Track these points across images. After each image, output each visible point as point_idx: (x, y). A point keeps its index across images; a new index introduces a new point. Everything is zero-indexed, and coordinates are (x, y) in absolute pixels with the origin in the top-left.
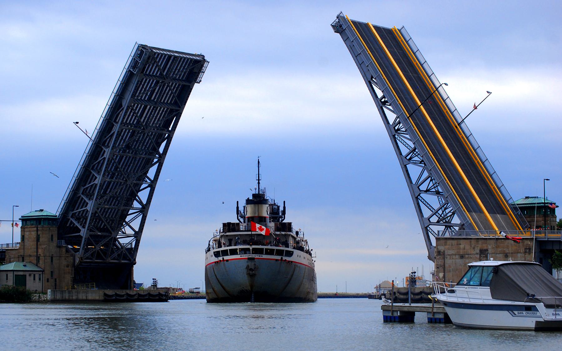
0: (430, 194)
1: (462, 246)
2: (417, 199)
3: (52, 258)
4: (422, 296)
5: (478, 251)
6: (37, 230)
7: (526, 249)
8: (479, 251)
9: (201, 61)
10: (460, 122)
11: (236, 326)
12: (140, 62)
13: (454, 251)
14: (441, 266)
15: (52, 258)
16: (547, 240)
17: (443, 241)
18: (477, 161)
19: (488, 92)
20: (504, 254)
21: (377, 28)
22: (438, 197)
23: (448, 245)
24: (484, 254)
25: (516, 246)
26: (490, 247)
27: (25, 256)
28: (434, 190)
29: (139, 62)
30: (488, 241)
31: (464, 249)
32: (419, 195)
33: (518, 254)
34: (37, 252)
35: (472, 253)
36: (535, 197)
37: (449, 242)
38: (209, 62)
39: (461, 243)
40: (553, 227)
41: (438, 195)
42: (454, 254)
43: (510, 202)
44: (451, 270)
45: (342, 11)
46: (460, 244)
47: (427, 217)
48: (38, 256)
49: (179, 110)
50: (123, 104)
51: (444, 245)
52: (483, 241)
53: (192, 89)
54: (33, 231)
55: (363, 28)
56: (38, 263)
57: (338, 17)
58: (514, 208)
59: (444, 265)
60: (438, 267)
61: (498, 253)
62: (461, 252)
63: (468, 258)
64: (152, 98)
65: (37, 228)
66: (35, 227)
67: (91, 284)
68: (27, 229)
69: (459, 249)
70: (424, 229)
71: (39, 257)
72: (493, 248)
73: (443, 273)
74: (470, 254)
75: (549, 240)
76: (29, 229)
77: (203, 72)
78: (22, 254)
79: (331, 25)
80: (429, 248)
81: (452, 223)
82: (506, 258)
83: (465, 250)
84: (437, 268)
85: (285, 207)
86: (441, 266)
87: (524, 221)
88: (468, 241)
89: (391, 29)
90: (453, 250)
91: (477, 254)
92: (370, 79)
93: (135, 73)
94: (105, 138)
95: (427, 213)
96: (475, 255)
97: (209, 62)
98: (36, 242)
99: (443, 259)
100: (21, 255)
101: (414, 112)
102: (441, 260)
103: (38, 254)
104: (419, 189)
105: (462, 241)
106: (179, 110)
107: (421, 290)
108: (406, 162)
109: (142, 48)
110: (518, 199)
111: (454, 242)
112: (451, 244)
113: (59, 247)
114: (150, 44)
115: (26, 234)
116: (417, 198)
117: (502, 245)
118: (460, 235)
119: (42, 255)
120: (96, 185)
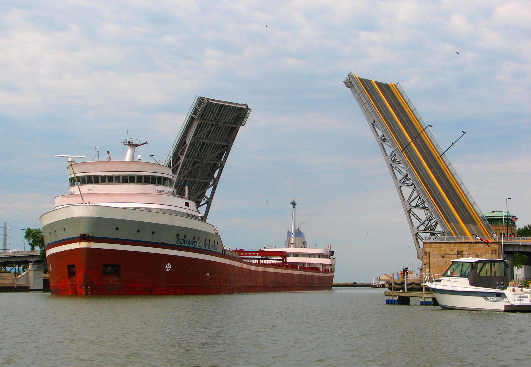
1: (443, 249)
5: (456, 252)
7: (492, 251)
9: (245, 109)
12: (200, 110)
13: (437, 252)
21: (378, 84)
22: (425, 211)
24: (460, 255)
26: (464, 249)
28: (421, 206)
31: (445, 251)
37: (434, 245)
38: (251, 110)
41: (425, 210)
43: (480, 215)
46: (442, 247)
49: (229, 146)
55: (366, 83)
57: (348, 76)
63: (448, 257)
77: (246, 117)
83: (446, 252)
88: (448, 244)
90: (437, 251)
92: (372, 122)
93: (196, 118)
95: (416, 223)
97: (251, 110)
108: (400, 185)
109: (201, 99)
110: (487, 213)
114: (207, 96)
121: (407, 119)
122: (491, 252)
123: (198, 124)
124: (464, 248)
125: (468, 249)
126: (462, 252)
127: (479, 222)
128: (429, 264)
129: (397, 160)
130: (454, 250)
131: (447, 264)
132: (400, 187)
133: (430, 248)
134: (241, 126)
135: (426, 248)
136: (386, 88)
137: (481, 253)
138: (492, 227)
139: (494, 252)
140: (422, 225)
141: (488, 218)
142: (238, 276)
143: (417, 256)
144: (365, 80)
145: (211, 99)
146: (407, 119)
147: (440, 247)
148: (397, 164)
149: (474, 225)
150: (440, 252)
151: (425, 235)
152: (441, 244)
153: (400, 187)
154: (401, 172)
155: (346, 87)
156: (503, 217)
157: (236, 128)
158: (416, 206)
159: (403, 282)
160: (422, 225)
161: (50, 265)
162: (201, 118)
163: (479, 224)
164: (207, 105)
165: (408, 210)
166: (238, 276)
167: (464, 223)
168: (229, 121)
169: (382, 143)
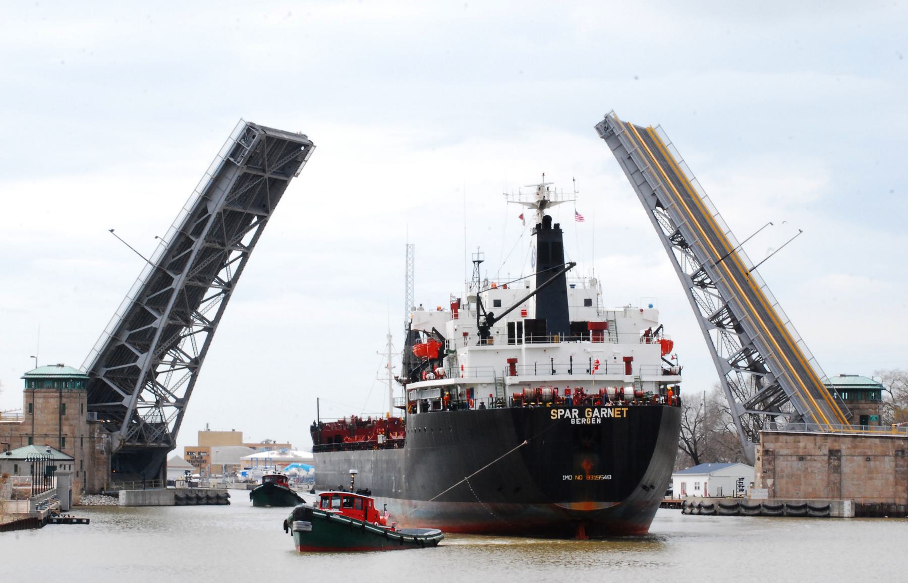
1: (802, 445)
3: (82, 438)
4: (761, 510)
5: (826, 452)
6: (61, 397)
7: (897, 451)
12: (249, 148)
13: (789, 450)
15: (82, 438)
17: (772, 437)
18: (779, 323)
19: (800, 230)
20: (866, 457)
23: (781, 442)
24: (835, 456)
26: (843, 447)
27: (34, 436)
29: (247, 149)
30: (842, 439)
31: (805, 448)
33: (886, 457)
34: (60, 430)
35: (817, 454)
36: (856, 376)
37: (782, 438)
39: (801, 441)
40: (592, 374)
42: (790, 454)
44: (785, 476)
45: (660, 124)
46: (799, 442)
48: (62, 436)
50: (210, 210)
51: (774, 441)
52: (834, 438)
54: (52, 398)
56: (62, 448)
60: (765, 471)
61: (856, 455)
62: (801, 452)
63: (810, 460)
65: (61, 393)
66: (56, 392)
67: (135, 483)
68: (39, 394)
69: (798, 448)
71: (64, 439)
72: (848, 448)
73: (773, 480)
74: (815, 456)
76: (43, 394)
77: (305, 161)
78: (29, 431)
82: (869, 462)
83: (806, 450)
84: (764, 472)
85: (520, 382)
88: (812, 438)
90: (789, 448)
91: (825, 455)
94: (173, 258)
96: (822, 457)
98: (58, 415)
100: (27, 434)
103: (62, 433)
105: (801, 438)
106: (266, 217)
107: (760, 503)
111: (790, 439)
112: (785, 441)
113: (90, 422)
114: (259, 122)
115: (38, 401)
117: (862, 444)
118: (793, 429)
119: (69, 434)
120: (155, 330)
122: (894, 453)
124: (842, 445)
126: (839, 451)
128: (774, 471)
130: (823, 447)
137: (874, 454)
138: (846, 404)
141: (837, 387)
142: (871, 498)
147: (795, 442)
149: (822, 401)
150: (796, 450)
152: (796, 437)
156: (454, 313)
161: (609, 477)
166: (871, 498)
167: (814, 398)
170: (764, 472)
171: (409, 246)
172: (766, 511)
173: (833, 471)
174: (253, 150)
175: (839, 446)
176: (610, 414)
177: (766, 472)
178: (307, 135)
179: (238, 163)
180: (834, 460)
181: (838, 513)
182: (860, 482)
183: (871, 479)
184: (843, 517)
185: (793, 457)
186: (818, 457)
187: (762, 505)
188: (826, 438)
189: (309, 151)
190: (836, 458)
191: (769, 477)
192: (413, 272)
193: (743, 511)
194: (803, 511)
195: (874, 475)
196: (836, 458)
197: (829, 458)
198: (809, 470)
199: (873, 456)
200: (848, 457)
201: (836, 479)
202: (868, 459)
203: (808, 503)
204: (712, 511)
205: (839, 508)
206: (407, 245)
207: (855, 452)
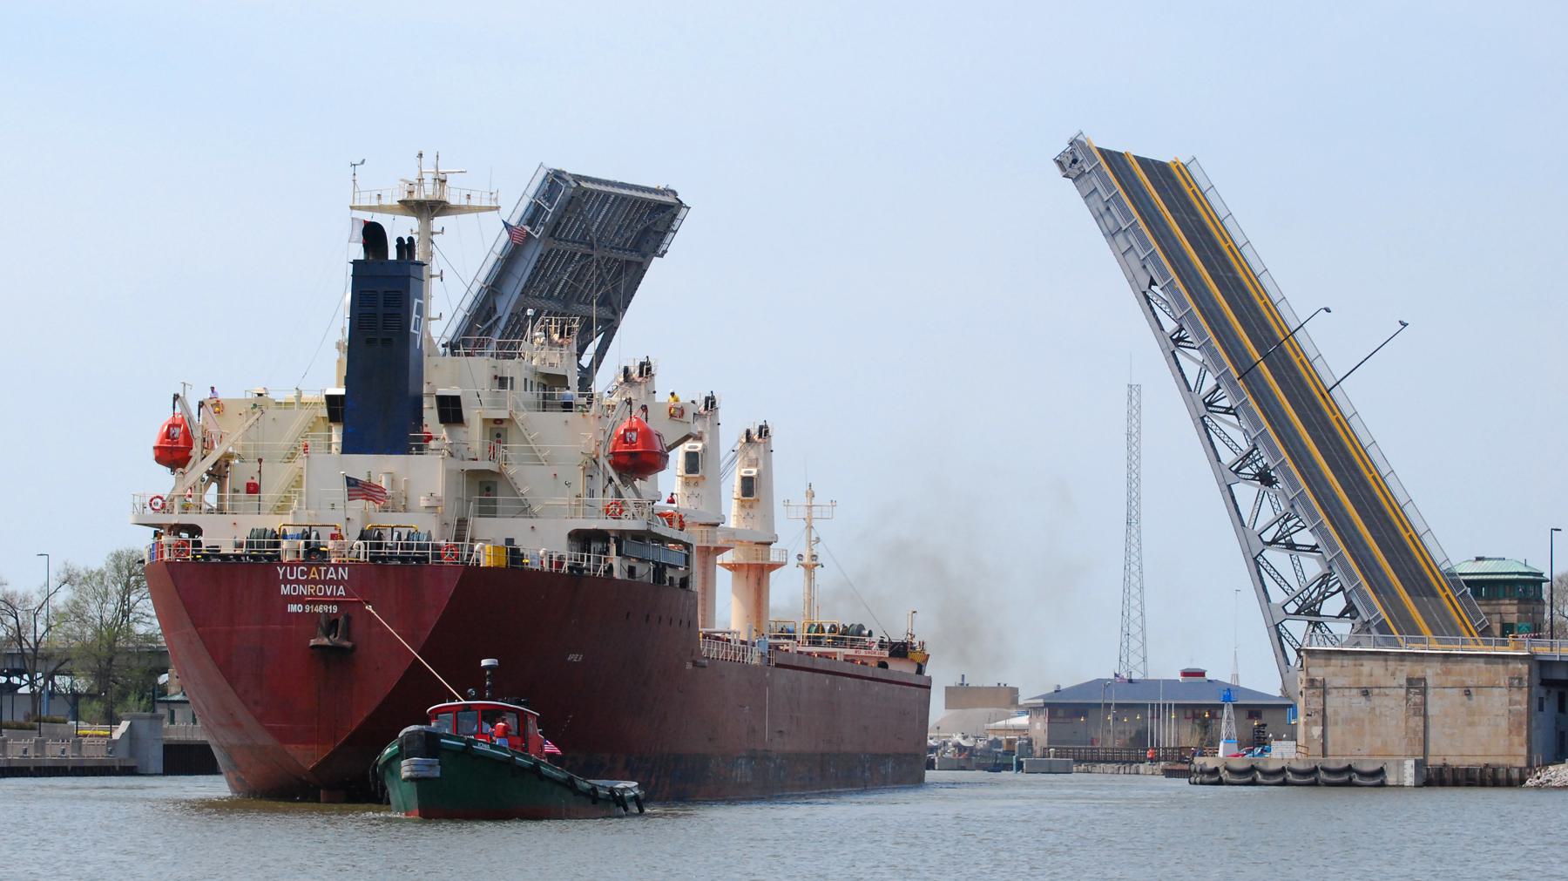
0: (1276, 549)
2: (1256, 563)
5: (1404, 682)
7: (1511, 678)
8: (1405, 681)
9: (673, 207)
10: (1330, 387)
11: (983, 834)
12: (551, 211)
14: (1317, 712)
16: (1558, 659)
20: (1464, 689)
21: (1142, 162)
22: (1291, 555)
24: (1416, 688)
25: (1490, 672)
28: (1283, 541)
29: (548, 212)
31: (1371, 675)
32: (1260, 554)
36: (1500, 559)
38: (689, 208)
41: (1292, 552)
43: (1444, 568)
47: (1279, 602)
49: (613, 320)
53: (645, 271)
55: (1115, 160)
57: (1071, 144)
58: (1452, 578)
59: (1324, 710)
62: (1365, 683)
63: (1378, 695)
64: (556, 294)
69: (1360, 674)
70: (1273, 629)
72: (1438, 674)
75: (1563, 659)
77: (673, 231)
79: (1055, 159)
80: (1284, 671)
81: (1321, 614)
83: (1373, 679)
84: (1308, 715)
86: (1317, 712)
87: (1474, 612)
89: (1168, 164)
90: (1345, 676)
92: (1145, 288)
93: (537, 236)
95: (1277, 596)
97: (689, 208)
99: (1322, 697)
101: (1247, 372)
102: (1316, 699)
104: (1262, 539)
107: (1285, 764)
108: (1231, 477)
109: (556, 176)
110: (1465, 566)
114: (572, 167)
116: (1257, 564)
118: (1358, 644)
121: (1230, 275)
123: (542, 255)
125: (1440, 672)
127: (1445, 594)
129: (1215, 404)
130: (1398, 673)
131: (1376, 716)
132: (1229, 485)
133: (1326, 666)
134: (655, 258)
135: (1315, 666)
136: (1160, 172)
139: (1517, 681)
140: (1293, 602)
141: (1467, 577)
143: (1281, 690)
144: (1107, 151)
145: (587, 179)
146: (1230, 275)
148: (1217, 414)
149: (1432, 599)
150: (1357, 678)
151: (1298, 629)
153: (1229, 485)
154: (1226, 439)
155: (1064, 176)
157: (641, 263)
158: (1274, 541)
159: (1253, 766)
160: (1293, 602)
162: (552, 235)
163: (1442, 595)
164: (573, 197)
165: (1255, 556)
167: (1410, 595)
168: (623, 245)
169: (1173, 353)
170: (1308, 715)
171: (1133, 387)
172: (1323, 776)
173: (1412, 712)
174: (560, 213)
175: (1422, 672)
176: (344, 572)
177: (1311, 715)
178: (677, 191)
179: (537, 233)
180: (1416, 693)
181: (1395, 780)
182: (1456, 731)
183: (1472, 724)
184: (1403, 786)
185: (1352, 690)
186: (1392, 689)
187: (1319, 767)
188: (1403, 658)
189: (675, 215)
190: (1417, 691)
191: (1316, 723)
192: (1139, 431)
193: (1356, 779)
194: (1345, 777)
195: (1476, 718)
196: (1417, 691)
197: (1408, 692)
198: (1377, 712)
199: (1475, 687)
200: (1437, 690)
201: (1417, 726)
202: (1468, 693)
203: (1352, 764)
204: (1215, 779)
205: (1398, 771)
206: (1130, 386)
207: (1447, 680)
